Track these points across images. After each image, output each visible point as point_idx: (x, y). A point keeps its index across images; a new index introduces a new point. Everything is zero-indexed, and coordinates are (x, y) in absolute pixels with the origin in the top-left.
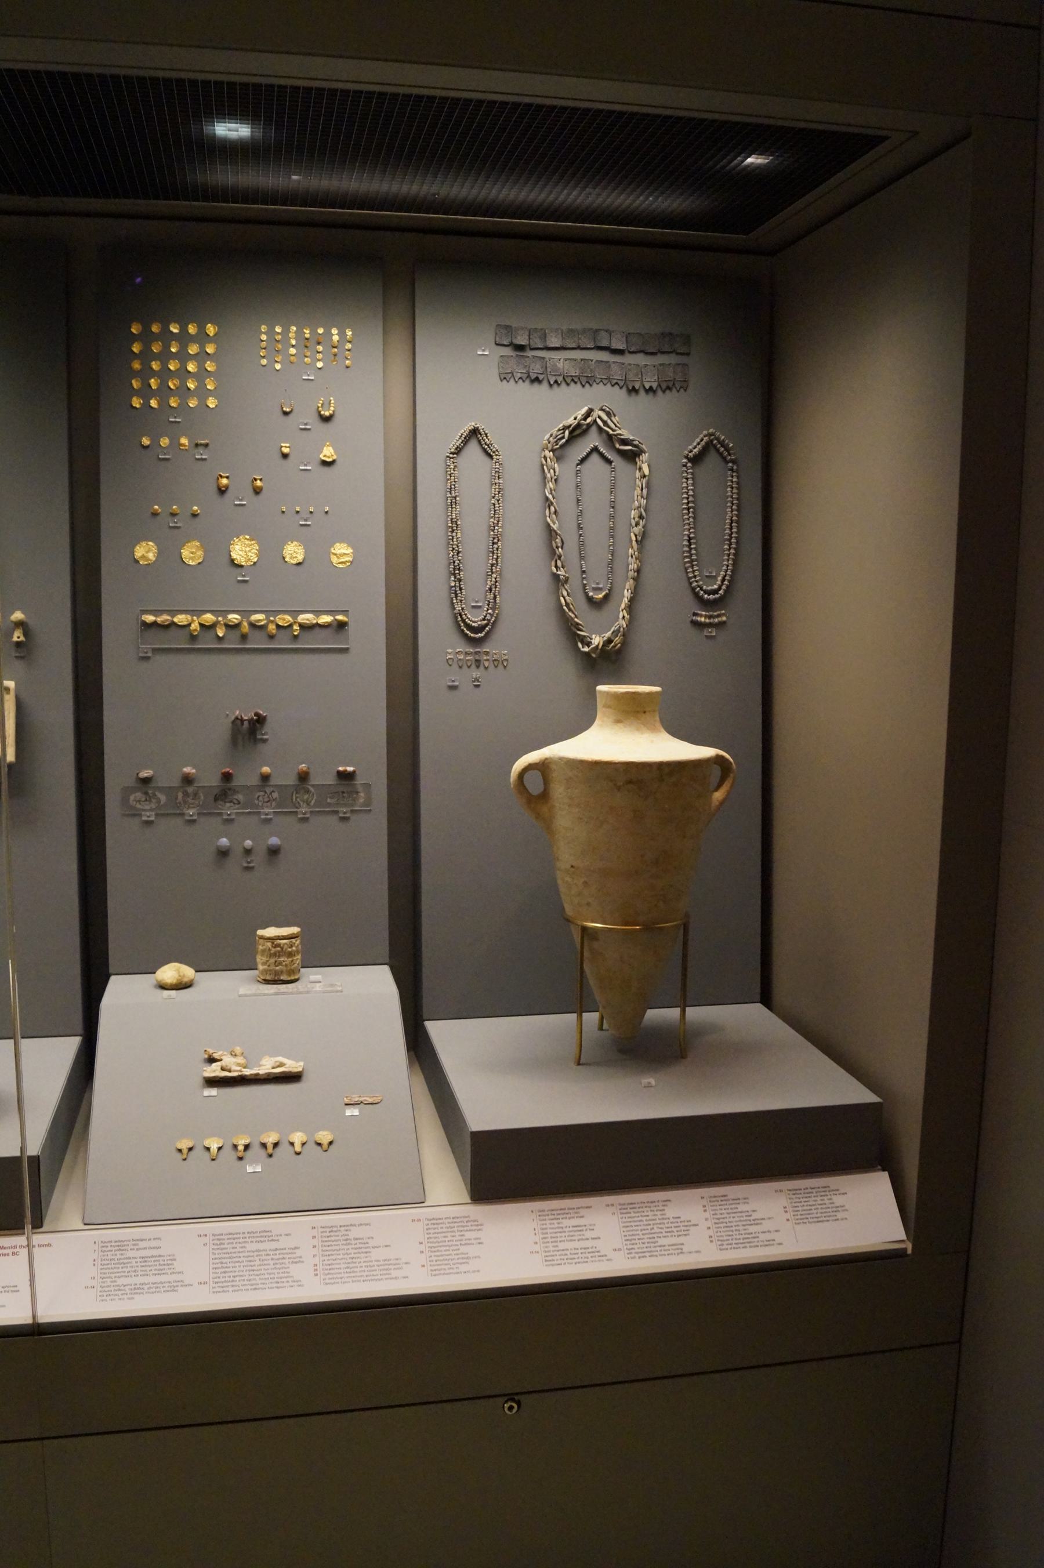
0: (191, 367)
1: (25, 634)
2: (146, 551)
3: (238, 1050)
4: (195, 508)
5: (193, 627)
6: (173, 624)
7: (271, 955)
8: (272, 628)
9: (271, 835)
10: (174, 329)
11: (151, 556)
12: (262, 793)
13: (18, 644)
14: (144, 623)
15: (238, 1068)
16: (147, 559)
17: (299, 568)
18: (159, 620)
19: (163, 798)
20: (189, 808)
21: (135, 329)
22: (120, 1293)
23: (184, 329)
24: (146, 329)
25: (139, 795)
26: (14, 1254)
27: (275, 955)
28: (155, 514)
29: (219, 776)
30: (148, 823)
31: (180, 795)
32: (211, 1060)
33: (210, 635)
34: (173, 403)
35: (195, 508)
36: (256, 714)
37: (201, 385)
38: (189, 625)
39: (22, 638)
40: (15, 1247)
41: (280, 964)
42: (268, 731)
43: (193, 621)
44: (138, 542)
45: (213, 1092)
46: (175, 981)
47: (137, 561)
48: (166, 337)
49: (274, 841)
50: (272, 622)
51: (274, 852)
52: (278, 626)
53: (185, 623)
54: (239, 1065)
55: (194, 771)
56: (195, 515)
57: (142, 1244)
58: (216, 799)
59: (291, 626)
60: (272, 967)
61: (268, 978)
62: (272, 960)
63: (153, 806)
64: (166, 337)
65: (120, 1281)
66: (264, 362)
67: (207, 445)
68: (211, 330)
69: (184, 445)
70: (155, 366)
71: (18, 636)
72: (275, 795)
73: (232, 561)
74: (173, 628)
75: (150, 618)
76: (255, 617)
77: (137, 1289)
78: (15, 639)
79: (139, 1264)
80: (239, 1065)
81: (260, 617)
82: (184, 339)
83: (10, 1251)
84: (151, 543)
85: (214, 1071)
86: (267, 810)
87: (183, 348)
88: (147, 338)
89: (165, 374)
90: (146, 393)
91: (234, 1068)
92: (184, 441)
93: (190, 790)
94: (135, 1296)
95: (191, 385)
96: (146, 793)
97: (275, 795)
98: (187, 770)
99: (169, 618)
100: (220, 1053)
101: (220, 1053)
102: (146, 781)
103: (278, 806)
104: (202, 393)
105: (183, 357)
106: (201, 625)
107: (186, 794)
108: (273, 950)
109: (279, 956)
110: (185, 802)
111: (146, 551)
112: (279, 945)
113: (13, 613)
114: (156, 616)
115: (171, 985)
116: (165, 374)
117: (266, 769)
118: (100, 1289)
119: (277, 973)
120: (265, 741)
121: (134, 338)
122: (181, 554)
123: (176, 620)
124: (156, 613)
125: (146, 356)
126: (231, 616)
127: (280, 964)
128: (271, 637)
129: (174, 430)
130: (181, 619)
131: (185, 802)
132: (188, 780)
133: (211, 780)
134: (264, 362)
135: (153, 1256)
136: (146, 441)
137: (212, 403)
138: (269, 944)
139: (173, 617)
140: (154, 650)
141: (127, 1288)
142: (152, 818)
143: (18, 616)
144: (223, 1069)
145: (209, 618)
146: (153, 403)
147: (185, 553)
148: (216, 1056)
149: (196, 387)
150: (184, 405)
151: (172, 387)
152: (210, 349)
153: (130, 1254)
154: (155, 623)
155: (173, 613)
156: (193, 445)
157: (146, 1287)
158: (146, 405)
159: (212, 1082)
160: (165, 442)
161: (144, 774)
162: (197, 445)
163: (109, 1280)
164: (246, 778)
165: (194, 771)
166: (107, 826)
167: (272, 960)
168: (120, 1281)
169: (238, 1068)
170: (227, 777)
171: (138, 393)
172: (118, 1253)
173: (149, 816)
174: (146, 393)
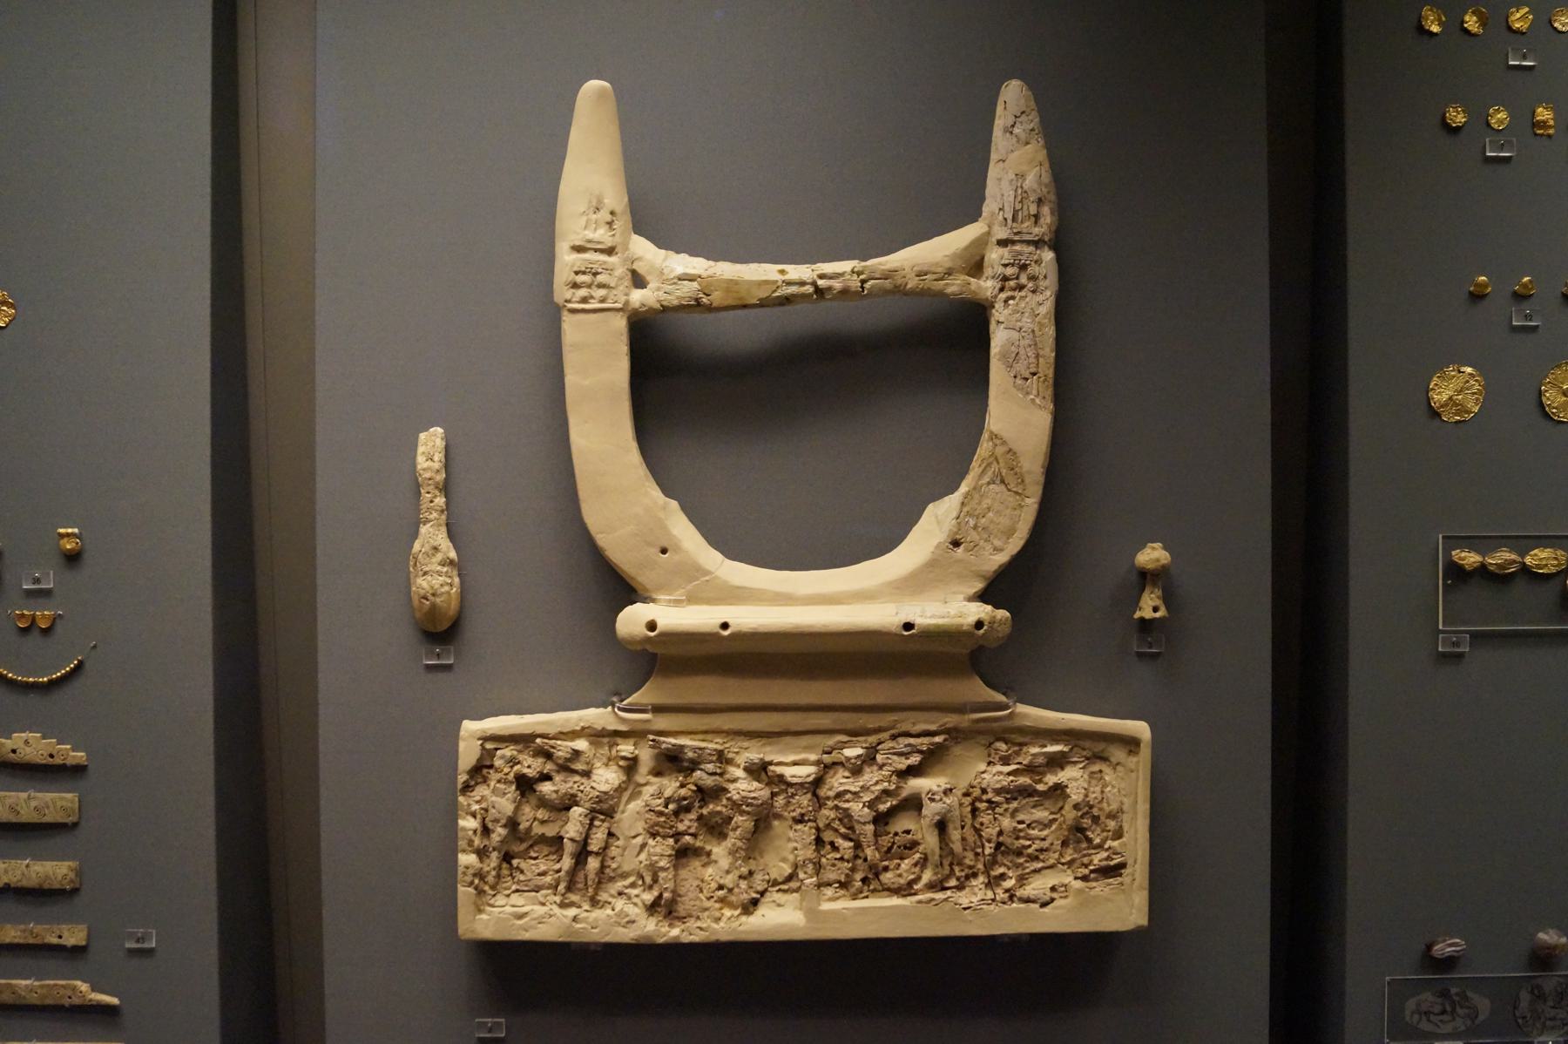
2: (1455, 388)
14: (1456, 573)
16: (1463, 409)
19: (1483, 1005)
25: (1427, 997)
28: (1477, 297)
31: (1525, 997)
44: (1439, 367)
47: (1435, 414)
63: (1460, 1024)
69: (1543, 125)
71: (1149, 606)
73: (1541, 405)
75: (1469, 558)
96: (1445, 994)
98: (1547, 937)
107: (1539, 995)
111: (1455, 388)
113: (1141, 546)
136: (1457, 117)
139: (1523, 554)
140: (1476, 637)
143: (1152, 555)
155: (1524, 543)
160: (1499, 118)
161: (1442, 949)
166: (209, 365)
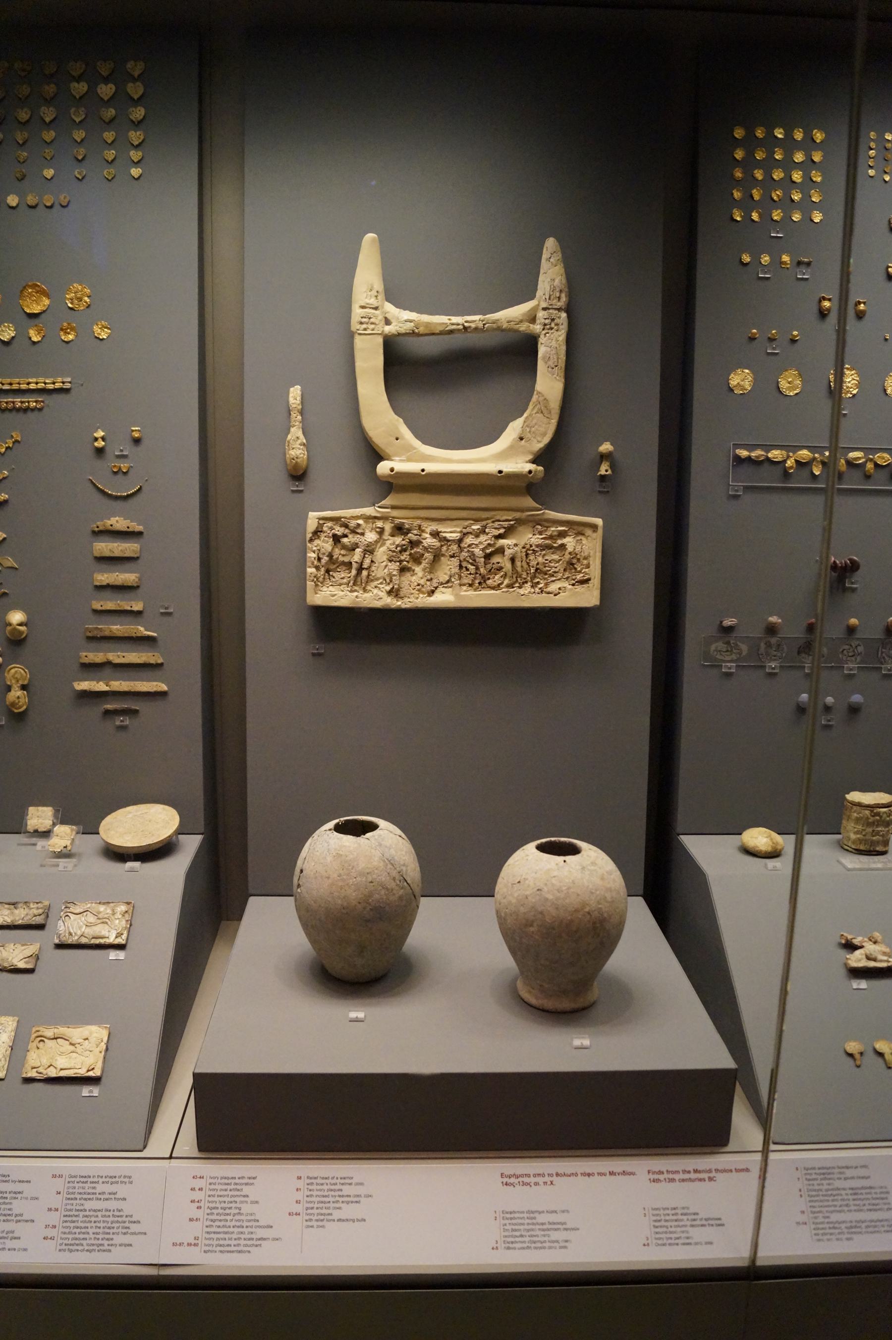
0: (797, 176)
1: (612, 467)
2: (741, 379)
3: (877, 935)
4: (795, 333)
5: (789, 463)
6: (768, 459)
7: (869, 824)
8: (870, 466)
9: (853, 692)
10: (779, 134)
11: (748, 385)
12: (847, 647)
13: (603, 477)
14: (739, 460)
15: (885, 958)
17: (64, 344)
18: (753, 454)
20: (771, 660)
21: (739, 133)
22: (837, 1231)
23: (789, 135)
24: (750, 133)
25: (720, 645)
26: (710, 1179)
27: (872, 824)
28: (752, 339)
29: (805, 625)
30: (728, 675)
31: (763, 645)
32: (850, 947)
33: (805, 473)
34: (777, 215)
35: (795, 333)
36: (850, 560)
37: (807, 196)
38: (785, 461)
39: (609, 472)
40: (710, 1171)
41: (878, 833)
42: (857, 581)
43: (788, 457)
45: (863, 984)
46: (770, 849)
47: (731, 390)
48: (771, 142)
49: (857, 698)
50: (871, 460)
51: (854, 710)
52: (877, 465)
53: (780, 460)
54: (884, 954)
55: (780, 621)
56: (793, 341)
57: (849, 1173)
58: (799, 653)
59: (865, 464)
60: (868, 837)
61: (862, 847)
62: (870, 830)
63: (734, 657)
64: (771, 142)
65: (834, 1217)
66: (871, 172)
67: (808, 264)
68: (819, 136)
69: (785, 263)
70: (759, 175)
72: (860, 649)
74: (766, 465)
75: (744, 453)
76: (852, 455)
77: (854, 1228)
78: (602, 472)
79: (850, 1197)
80: (884, 954)
81: (805, 452)
82: (789, 145)
83: (705, 1176)
84: (747, 371)
85: (857, 959)
86: (851, 666)
87: (750, 154)
88: (750, 143)
89: (769, 183)
90: (748, 203)
91: (881, 957)
92: (785, 258)
93: (773, 640)
94: (854, 1236)
95: (796, 197)
96: (728, 643)
97: (860, 649)
98: (774, 619)
99: (763, 453)
100: (860, 939)
101: (860, 939)
102: (728, 630)
103: (862, 662)
104: (807, 206)
105: (788, 165)
106: (797, 461)
107: (769, 645)
108: (871, 820)
109: (877, 826)
110: (767, 654)
111: (741, 379)
112: (878, 814)
113: (601, 445)
114: (750, 451)
115: (766, 852)
116: (769, 183)
117: (854, 621)
118: (813, 1226)
119: (873, 843)
120: (854, 590)
121: (737, 143)
122: (778, 382)
123: (770, 455)
124: (751, 447)
125: (749, 164)
126: (852, 455)
127: (878, 833)
128: (868, 477)
129: (775, 247)
130: (776, 454)
131: (767, 654)
132: (771, 630)
133: (795, 632)
134: (871, 172)
135: (863, 1188)
136: (746, 258)
137: (817, 217)
138: (867, 812)
139: (768, 451)
141: (843, 1226)
142: (733, 670)
143: (606, 447)
144: (869, 958)
145: (804, 454)
146: (755, 216)
147: (783, 384)
148: (856, 941)
149: (801, 199)
150: (787, 218)
151: (775, 198)
152: (817, 157)
153: (838, 1184)
154: (749, 458)
155: (768, 448)
156: (795, 263)
157: (864, 1225)
158: (747, 217)
159: (857, 973)
160: (765, 259)
161: (727, 622)
162: (799, 263)
163: (821, 1215)
164: (833, 631)
165: (780, 621)
167: (870, 830)
168: (834, 1217)
169: (885, 958)
170: (811, 628)
171: (738, 204)
172: (825, 1182)
173: (730, 666)
174: (748, 203)
